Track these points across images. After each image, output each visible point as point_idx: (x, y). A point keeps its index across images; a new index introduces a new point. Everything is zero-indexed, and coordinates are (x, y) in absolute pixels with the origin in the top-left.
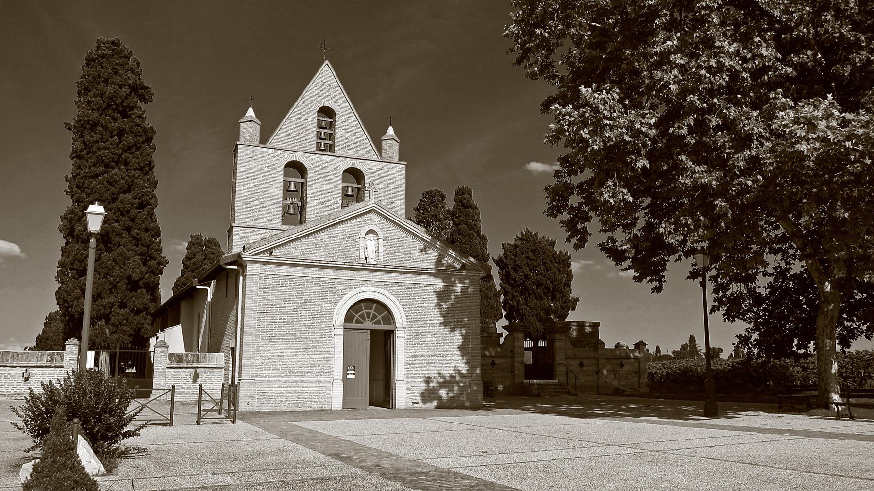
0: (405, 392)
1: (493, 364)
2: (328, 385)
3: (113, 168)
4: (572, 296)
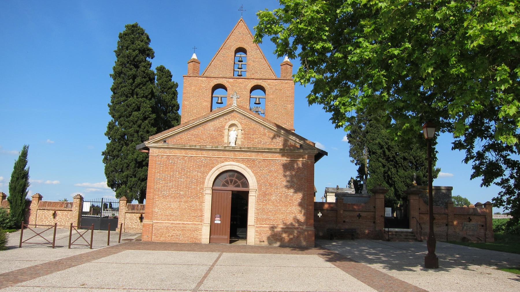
0: (254, 233)
1: (359, 216)
2: (200, 227)
3: (130, 97)
4: (435, 168)
